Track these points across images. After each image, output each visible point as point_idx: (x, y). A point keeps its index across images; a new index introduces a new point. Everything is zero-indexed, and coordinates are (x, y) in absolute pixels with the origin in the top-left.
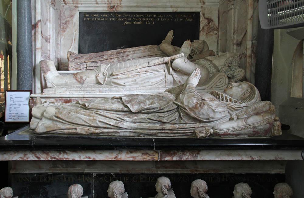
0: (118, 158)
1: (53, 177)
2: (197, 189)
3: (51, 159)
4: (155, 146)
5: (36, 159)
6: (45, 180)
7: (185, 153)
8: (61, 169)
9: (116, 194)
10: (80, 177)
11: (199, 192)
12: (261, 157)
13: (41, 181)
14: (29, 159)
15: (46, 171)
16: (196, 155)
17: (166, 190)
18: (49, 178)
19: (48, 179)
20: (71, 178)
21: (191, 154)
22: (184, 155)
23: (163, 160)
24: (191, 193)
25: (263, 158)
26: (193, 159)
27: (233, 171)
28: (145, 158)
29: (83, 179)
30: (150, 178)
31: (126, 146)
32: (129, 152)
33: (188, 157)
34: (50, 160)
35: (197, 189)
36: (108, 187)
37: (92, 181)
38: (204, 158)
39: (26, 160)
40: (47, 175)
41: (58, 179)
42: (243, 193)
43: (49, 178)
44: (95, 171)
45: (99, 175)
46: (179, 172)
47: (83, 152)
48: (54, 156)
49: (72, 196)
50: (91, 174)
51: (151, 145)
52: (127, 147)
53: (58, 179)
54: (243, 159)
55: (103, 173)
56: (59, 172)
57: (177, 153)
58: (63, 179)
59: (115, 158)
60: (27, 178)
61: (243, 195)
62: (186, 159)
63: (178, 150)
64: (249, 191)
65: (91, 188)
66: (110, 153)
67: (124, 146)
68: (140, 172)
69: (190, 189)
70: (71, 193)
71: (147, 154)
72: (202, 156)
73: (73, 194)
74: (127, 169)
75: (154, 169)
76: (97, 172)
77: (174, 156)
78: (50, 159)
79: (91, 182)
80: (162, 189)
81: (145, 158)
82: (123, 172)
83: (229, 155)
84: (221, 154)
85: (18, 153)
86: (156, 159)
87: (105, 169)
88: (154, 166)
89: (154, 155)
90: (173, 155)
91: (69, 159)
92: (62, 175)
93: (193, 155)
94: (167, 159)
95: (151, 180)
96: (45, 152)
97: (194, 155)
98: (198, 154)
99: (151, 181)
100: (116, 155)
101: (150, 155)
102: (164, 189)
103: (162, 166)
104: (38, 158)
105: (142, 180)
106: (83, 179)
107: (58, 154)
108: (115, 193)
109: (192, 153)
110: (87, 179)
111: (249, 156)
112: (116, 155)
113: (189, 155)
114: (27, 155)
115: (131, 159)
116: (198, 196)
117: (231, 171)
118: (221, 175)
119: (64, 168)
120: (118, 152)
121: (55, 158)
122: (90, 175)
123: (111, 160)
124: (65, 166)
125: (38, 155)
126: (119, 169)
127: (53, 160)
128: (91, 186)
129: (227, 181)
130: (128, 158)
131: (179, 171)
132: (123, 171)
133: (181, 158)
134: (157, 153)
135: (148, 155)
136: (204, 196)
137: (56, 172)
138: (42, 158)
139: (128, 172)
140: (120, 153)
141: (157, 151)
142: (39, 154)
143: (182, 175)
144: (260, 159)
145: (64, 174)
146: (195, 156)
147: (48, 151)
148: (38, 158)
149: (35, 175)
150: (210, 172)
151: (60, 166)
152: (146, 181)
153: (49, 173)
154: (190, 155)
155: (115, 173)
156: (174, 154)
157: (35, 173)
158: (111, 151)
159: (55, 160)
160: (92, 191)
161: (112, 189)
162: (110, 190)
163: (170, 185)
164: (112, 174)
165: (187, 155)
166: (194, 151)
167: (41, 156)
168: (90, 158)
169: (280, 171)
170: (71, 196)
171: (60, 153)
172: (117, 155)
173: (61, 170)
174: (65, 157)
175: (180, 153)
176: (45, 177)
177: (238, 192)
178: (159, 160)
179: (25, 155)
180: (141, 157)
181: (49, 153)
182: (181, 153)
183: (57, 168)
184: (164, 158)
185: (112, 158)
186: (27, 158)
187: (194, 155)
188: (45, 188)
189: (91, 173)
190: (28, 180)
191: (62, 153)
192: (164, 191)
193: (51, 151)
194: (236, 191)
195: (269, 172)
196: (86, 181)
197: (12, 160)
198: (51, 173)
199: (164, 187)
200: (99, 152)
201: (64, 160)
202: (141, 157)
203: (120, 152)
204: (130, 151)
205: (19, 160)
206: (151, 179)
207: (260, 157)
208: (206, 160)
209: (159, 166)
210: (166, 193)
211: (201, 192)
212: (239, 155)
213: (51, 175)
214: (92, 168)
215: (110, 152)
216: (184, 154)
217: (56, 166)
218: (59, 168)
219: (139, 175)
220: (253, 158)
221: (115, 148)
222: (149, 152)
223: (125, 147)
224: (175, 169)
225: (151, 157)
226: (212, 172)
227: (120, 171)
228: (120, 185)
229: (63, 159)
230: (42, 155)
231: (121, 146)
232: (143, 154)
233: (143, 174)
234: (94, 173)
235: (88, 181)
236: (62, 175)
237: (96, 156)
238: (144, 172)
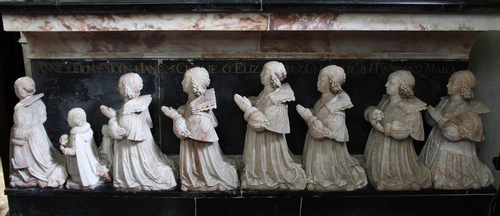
0: (200, 27)
1: (93, 66)
2: (329, 78)
3: (89, 29)
4: (263, 5)
5: (65, 30)
6: (82, 71)
7: (313, 19)
8: (107, 53)
9: (195, 86)
10: (136, 67)
11: (331, 83)
12: (437, 27)
13: (75, 72)
14: (53, 30)
15: (82, 56)
16: (330, 21)
17: (278, 80)
18: (88, 67)
19: (86, 69)
20: (122, 68)
21: (323, 21)
22: (310, 22)
23: (275, 29)
24: (318, 85)
25: (441, 28)
26: (325, 29)
27: (389, 55)
28: (245, 27)
29: (142, 69)
30: (251, 66)
31: (213, 4)
32: (219, 17)
33: (318, 24)
34: (87, 30)
35: (329, 78)
36: (182, 77)
37: (156, 72)
38: (344, 27)
39: (49, 30)
40: (83, 61)
41: (102, 69)
42: (401, 85)
43: (88, 67)
44: (160, 55)
45: (167, 63)
46: (299, 57)
47: (141, 17)
48: (93, 25)
49: (126, 90)
50: (154, 61)
51: (257, 3)
52: (215, 7)
53: (102, 69)
54: (407, 30)
55: (174, 60)
56: (104, 57)
57: (299, 19)
58: (110, 68)
59: (194, 27)
60: (53, 66)
61: (402, 87)
62: (314, 28)
63: (301, 14)
64: (411, 82)
65: (156, 84)
66: (185, 18)
67: (209, 4)
68: (235, 57)
69: (318, 80)
70: (123, 86)
71: (248, 19)
72: (340, 24)
73: (127, 87)
74: (213, 53)
75: (258, 52)
76: (165, 57)
77: (294, 24)
78: (86, 29)
79: (155, 73)
80: (271, 79)
81: (245, 27)
82: (207, 57)
83: (384, 22)
84: (372, 20)
85: (35, 20)
86: (263, 28)
87: (178, 53)
88: (259, 48)
89: (261, 22)
90: (292, 22)
91: (118, 29)
92: (108, 62)
93: (326, 22)
94: (283, 27)
95: (253, 70)
96: (78, 17)
97: (328, 22)
98: (335, 19)
99: (253, 72)
100: (196, 22)
101: (254, 22)
102: (276, 78)
103: (271, 48)
104: (68, 27)
105: (238, 69)
106: (142, 69)
107: (99, 21)
108: (194, 85)
109: (324, 19)
110: (148, 69)
111: (418, 25)
112: (196, 22)
113: (319, 22)
114: (49, 23)
115: (221, 28)
116: (329, 90)
117: (385, 56)
118: (368, 62)
119: (111, 52)
120: (198, 17)
121: (94, 27)
122: (153, 62)
123: (187, 29)
124: (111, 49)
125: (67, 24)
126: (201, 53)
127: (92, 30)
128: (155, 79)
129: (376, 72)
130: (217, 26)
131: (301, 55)
132: (207, 55)
133: (306, 27)
134: (266, 17)
135: (249, 21)
136: (338, 88)
137: (97, 57)
138: (74, 27)
139: (215, 58)
140: (202, 18)
141: (265, 14)
142: (68, 21)
143: (304, 62)
144: (436, 29)
145: (111, 60)
146: (330, 23)
147: (83, 17)
148: (68, 27)
149: (66, 63)
150: (350, 58)
151: (104, 49)
152: (245, 72)
153: (87, 60)
154: (321, 21)
155: (194, 59)
156: (295, 20)
157: (66, 60)
158: (187, 16)
159: (95, 30)
160: (156, 87)
161: (189, 79)
162: (187, 81)
163: (285, 73)
164: (188, 60)
165: (316, 22)
166: (328, 15)
167: (72, 24)
168: (152, 27)
169: (462, 55)
170: (125, 89)
171: (103, 20)
172: (197, 21)
173: (105, 55)
174: (111, 26)
175: (304, 19)
176: (81, 66)
177: (393, 84)
178: (268, 30)
179: (47, 23)
180: (238, 25)
181: (84, 19)
182: (305, 19)
183: (100, 52)
184: (277, 26)
185: (189, 27)
186: (51, 28)
187: (328, 22)
188: (83, 84)
189: (155, 58)
190: (56, 71)
191: (106, 19)
192: (275, 81)
193: (88, 16)
194: (391, 82)
195: (445, 58)
196: (147, 72)
197: (27, 30)
198: (91, 60)
199: (274, 76)
200: (168, 17)
201: (110, 30)
202: (238, 25)
203: (203, 16)
204: (219, 15)
205: (37, 30)
206: (253, 69)
207: (435, 26)
208: (346, 30)
209: (267, 47)
210: (278, 85)
211: (334, 82)
212: (402, 22)
213: (90, 63)
214: (155, 51)
215: (187, 17)
216: (311, 21)
217: (97, 48)
218: (102, 51)
219: (233, 62)
220: (424, 28)
221: (195, 8)
222: (251, 16)
223: (212, 5)
224: (293, 53)
225: (255, 24)
226: (354, 58)
227: (202, 55)
228: (203, 72)
229: (107, 29)
230: (73, 23)
231: (205, 4)
232: (241, 19)
233: (240, 60)
234: (160, 58)
235: (150, 72)
236: (108, 62)
237: (162, 23)
238: (241, 57)
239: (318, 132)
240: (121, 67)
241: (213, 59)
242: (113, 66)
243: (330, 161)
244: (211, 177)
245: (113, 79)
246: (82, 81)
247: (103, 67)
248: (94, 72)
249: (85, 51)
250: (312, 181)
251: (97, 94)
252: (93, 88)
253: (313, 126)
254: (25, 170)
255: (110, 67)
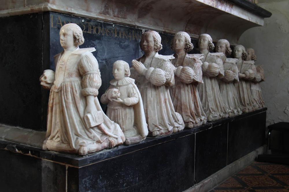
6: (95, 32)
13: (89, 32)
40: (95, 19)
124: (116, 14)
176: (94, 26)
177: (240, 51)
214: (141, 22)
239: (232, 76)
240: (121, 32)
241: (2, 124)
242: (117, 30)
243: (234, 96)
244: (169, 125)
245: (116, 43)
246: (94, 42)
247: (110, 31)
248: (103, 35)
249: (98, 11)
250: (230, 111)
251: (104, 57)
252: (101, 51)
253: (229, 73)
254: (99, 127)
255: (114, 31)
